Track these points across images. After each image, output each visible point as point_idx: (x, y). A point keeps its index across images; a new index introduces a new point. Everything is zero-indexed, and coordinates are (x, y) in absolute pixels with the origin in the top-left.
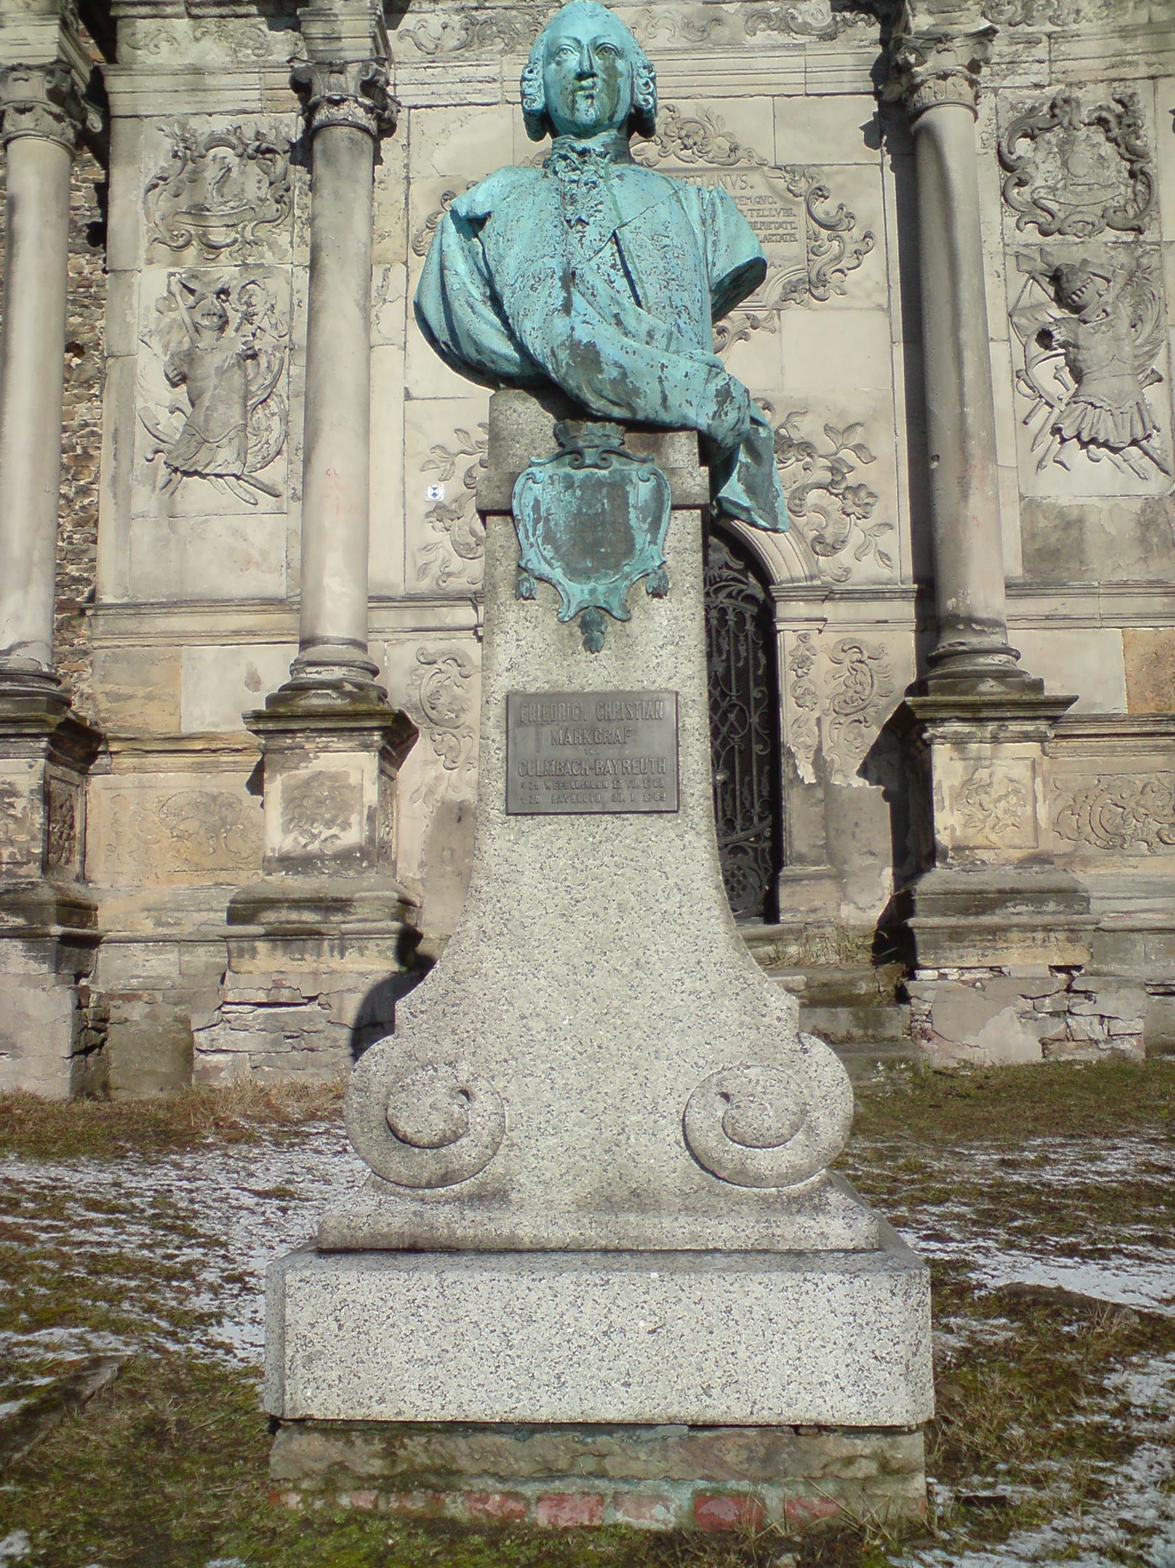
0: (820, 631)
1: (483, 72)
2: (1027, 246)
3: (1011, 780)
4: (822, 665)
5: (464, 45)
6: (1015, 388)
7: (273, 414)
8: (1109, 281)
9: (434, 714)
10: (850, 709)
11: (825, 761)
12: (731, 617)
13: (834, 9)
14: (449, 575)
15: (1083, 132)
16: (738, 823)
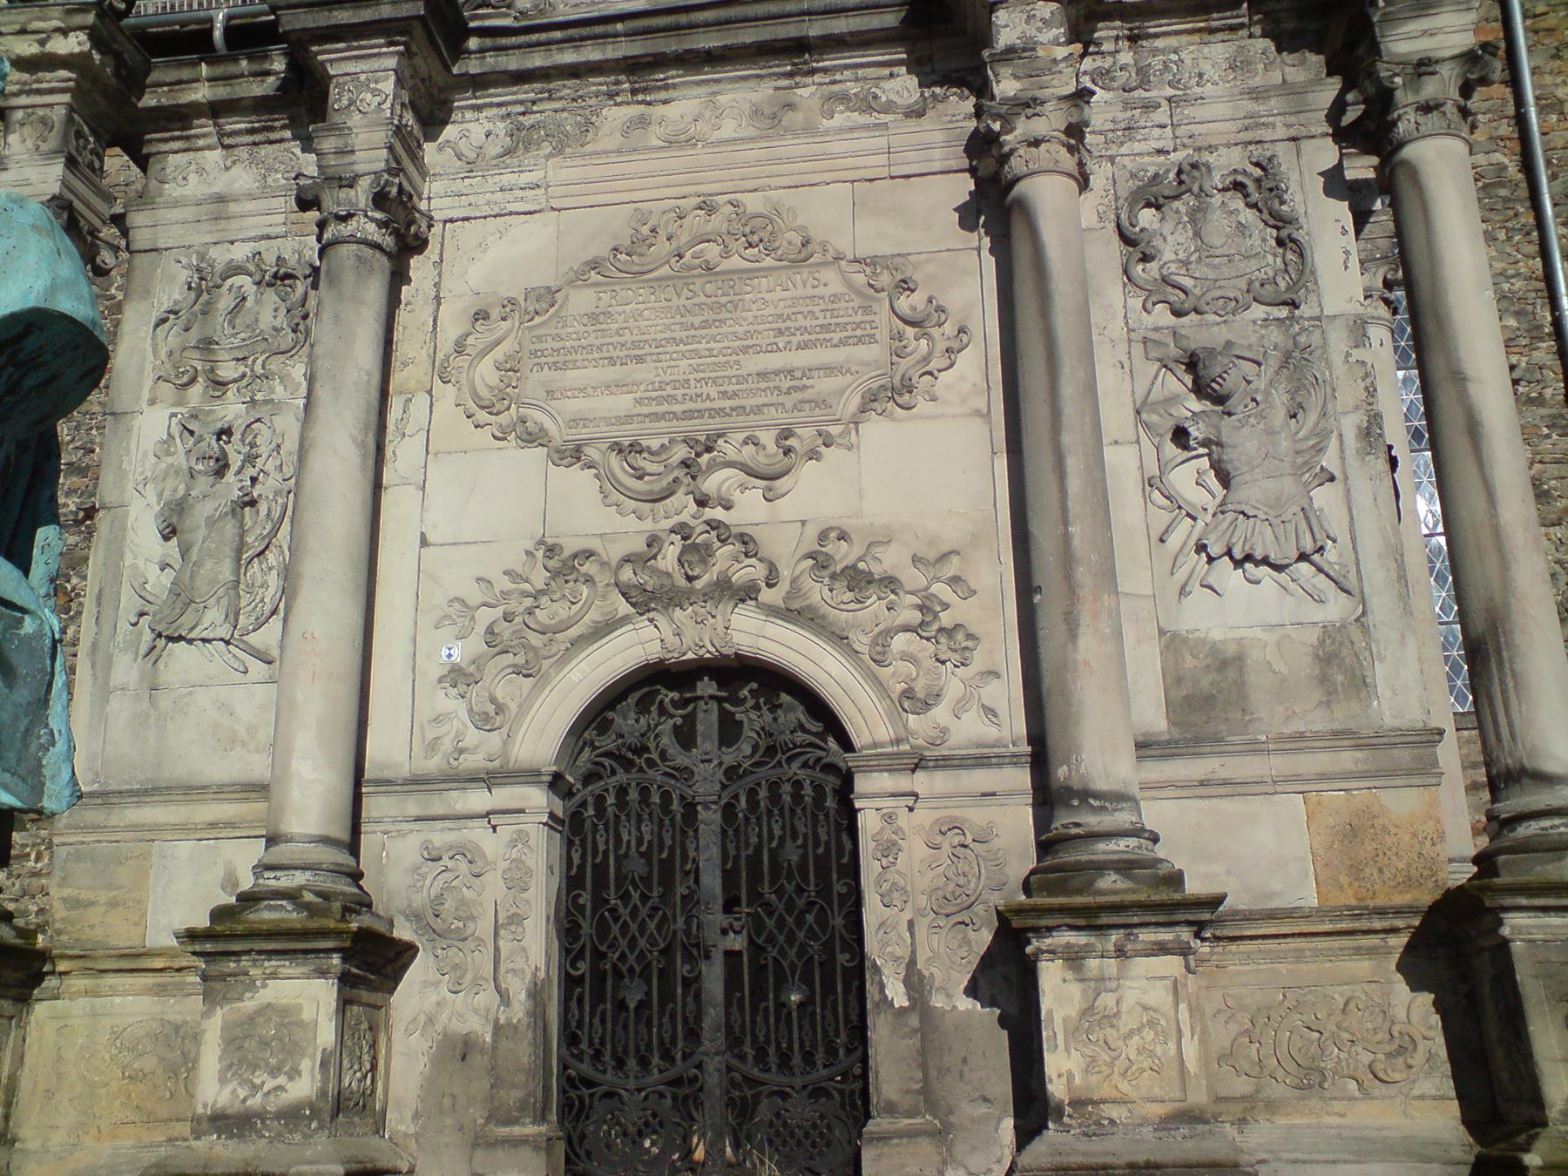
0: (911, 809)
1: (526, 178)
2: (1157, 329)
3: (1146, 1008)
4: (915, 851)
5: (508, 152)
6: (1146, 499)
7: (271, 569)
8: (1259, 364)
9: (437, 924)
10: (953, 909)
11: (921, 976)
12: (808, 791)
13: (921, 86)
14: (461, 751)
15: (1217, 199)
16: (820, 1057)
